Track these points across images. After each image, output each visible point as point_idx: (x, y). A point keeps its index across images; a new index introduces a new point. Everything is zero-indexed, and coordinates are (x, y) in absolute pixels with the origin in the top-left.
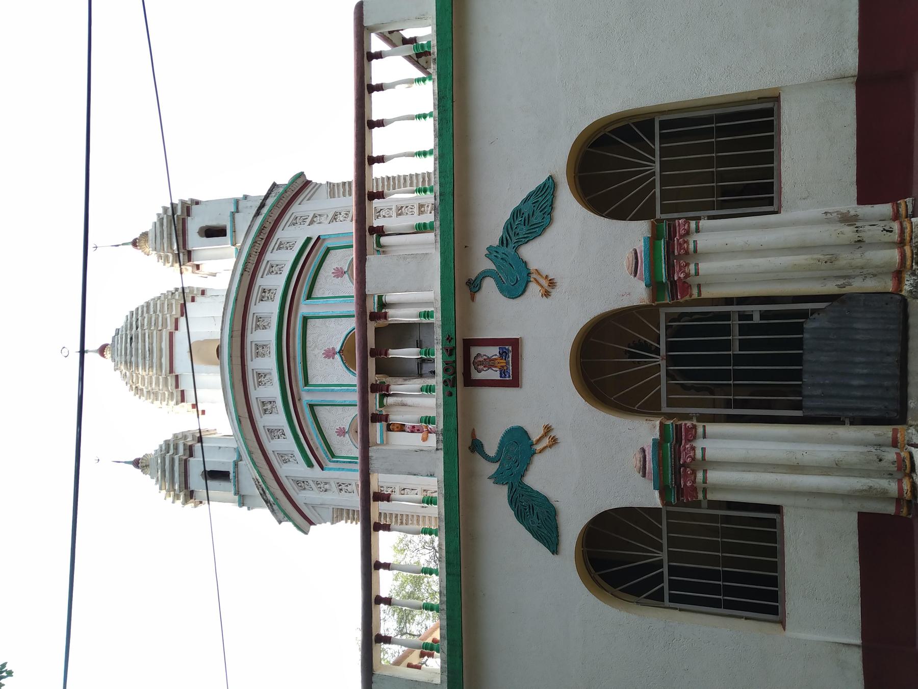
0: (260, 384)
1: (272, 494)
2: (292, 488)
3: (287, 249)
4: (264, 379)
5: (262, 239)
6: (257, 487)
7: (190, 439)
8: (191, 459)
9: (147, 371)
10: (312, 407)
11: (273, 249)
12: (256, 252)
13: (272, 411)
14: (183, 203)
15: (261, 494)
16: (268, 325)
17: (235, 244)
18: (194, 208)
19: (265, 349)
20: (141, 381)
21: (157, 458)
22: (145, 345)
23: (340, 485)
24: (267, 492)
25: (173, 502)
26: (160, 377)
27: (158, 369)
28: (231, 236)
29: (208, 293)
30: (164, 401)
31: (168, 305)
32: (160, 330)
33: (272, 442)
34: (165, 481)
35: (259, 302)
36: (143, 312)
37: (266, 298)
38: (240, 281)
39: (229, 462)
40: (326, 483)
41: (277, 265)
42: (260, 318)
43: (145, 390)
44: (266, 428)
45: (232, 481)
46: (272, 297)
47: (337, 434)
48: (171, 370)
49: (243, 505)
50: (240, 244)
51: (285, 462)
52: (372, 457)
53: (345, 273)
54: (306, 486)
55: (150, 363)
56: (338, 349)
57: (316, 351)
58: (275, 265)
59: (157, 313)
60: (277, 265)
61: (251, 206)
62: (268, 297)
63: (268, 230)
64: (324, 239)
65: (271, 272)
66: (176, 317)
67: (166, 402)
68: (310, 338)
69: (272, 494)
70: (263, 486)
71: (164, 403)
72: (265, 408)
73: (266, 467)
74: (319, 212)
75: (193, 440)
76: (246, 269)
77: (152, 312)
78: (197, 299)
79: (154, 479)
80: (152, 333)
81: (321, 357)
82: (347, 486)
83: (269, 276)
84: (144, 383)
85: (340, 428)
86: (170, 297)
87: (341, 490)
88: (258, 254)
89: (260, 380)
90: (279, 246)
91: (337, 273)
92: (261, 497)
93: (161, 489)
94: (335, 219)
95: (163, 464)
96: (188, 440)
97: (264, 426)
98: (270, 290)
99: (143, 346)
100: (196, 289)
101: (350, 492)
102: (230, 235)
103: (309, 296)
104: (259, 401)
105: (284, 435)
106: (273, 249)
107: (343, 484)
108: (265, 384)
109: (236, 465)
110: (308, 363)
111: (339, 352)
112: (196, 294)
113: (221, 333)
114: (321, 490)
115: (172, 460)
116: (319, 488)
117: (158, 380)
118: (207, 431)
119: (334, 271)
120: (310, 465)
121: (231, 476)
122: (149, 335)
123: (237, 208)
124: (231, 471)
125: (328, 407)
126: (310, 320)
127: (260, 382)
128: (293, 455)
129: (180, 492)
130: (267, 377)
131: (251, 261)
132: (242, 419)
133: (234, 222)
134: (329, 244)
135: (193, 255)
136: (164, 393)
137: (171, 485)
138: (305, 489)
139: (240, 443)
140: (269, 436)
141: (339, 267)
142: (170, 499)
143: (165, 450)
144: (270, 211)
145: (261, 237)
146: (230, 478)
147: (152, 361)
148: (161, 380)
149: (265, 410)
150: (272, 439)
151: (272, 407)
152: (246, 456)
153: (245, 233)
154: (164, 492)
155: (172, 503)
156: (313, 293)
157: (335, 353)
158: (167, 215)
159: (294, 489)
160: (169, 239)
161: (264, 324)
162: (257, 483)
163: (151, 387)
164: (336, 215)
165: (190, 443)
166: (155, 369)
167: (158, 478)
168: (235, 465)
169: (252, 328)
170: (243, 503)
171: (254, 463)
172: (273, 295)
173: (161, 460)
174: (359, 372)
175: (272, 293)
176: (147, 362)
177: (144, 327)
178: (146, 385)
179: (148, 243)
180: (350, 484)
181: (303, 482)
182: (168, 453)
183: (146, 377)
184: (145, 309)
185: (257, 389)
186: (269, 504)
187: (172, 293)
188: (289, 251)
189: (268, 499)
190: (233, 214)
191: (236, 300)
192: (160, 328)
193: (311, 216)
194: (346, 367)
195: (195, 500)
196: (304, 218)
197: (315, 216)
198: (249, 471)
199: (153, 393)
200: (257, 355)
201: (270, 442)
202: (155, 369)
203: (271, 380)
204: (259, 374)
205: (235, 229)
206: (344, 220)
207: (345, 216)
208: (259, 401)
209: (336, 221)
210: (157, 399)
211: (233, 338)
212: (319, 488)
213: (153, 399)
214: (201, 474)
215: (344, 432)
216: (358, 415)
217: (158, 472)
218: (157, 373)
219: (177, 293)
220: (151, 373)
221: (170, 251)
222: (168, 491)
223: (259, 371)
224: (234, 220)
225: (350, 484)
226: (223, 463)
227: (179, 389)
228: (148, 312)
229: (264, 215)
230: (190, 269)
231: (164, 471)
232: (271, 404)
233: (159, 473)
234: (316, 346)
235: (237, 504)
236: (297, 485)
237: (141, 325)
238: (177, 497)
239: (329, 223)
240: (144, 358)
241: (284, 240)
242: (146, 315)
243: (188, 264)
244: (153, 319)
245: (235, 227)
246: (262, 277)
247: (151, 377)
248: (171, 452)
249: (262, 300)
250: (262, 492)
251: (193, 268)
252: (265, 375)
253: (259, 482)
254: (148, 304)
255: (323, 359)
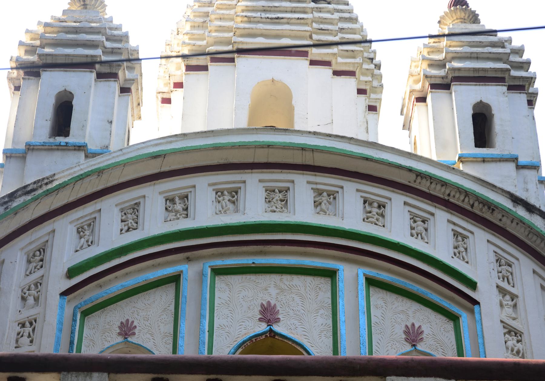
0: (219, 194)
1: (25, 206)
2: (33, 239)
3: (456, 248)
4: (226, 201)
5: (472, 206)
6: (39, 181)
7: (129, 75)
8: (94, 75)
9: (242, 14)
10: (175, 279)
11: (454, 224)
12: (449, 195)
13: (171, 211)
14: (531, 80)
15: (25, 187)
16: (322, 210)
17: (462, 161)
18: (521, 98)
19: (279, 204)
20: (225, 4)
21: (100, 21)
22: (286, 12)
23: (31, 324)
24: (29, 197)
25: (21, 44)
26: (231, 34)
27: (247, 31)
28: (476, 154)
29: (371, 116)
30: (190, 39)
31: (352, 51)
32: (311, 37)
33: (116, 211)
34: (59, 32)
35: (361, 197)
36: (342, 11)
37: (368, 209)
38: (400, 167)
39: (84, 137)
40: (36, 299)
41: (426, 230)
42: (335, 198)
43: (210, 9)
44: (141, 200)
45: (52, 140)
46: (370, 219)
47: (124, 321)
48: (241, 52)
49: (7, 157)
50: (461, 169)
51: (80, 231)
52: (91, 377)
53: (414, 345)
54: (35, 264)
55: (256, 19)
56: (277, 328)
57: (273, 291)
58: (426, 226)
59: (339, 34)
60: (426, 230)
61: (527, 190)
62: (370, 212)
63: (487, 215)
64: (472, 312)
65: (414, 218)
66: (333, 62)
67: (187, 41)
68: (297, 281)
69: (25, 206)
70: (40, 191)
71: (186, 39)
72: (177, 200)
73: (72, 198)
74: (520, 305)
75: (126, 80)
76: (419, 178)
77: (341, 25)
78: (362, 97)
79: (63, 14)
80: (306, 24)
81: (263, 298)
82: (29, 336)
83: (408, 216)
84: (221, 9)
85: (135, 327)
86: (366, 55)
87: (23, 325)
88: (447, 198)
89: (226, 193)
90: (461, 234)
91: (414, 332)
92: (21, 186)
93: (46, 25)
94: (509, 332)
95: (90, 30)
96: (126, 72)
97: (144, 197)
98: (383, 216)
99: (285, 9)
100: (378, 96)
101: (17, 341)
102: (477, 152)
103: (371, 282)
104: (190, 190)
105: (128, 230)
106: (454, 224)
107: (34, 330)
108: (219, 202)
109: (80, 148)
110: (253, 277)
111: (271, 331)
112: (369, 97)
113: (310, 132)
114: (25, 291)
115: (93, 45)
116: (30, 286)
117: (228, 29)
118: (139, 104)
119: (417, 326)
120: (71, 273)
121: (61, 140)
122: (303, 19)
123: (524, 167)
124: (70, 140)
125: (172, 307)
126: (330, 282)
127: (222, 193)
128: (90, 244)
129: (40, 56)
130: (231, 206)
131: (433, 186)
132: (159, 160)
133: (500, 161)
134: (465, 319)
135: (442, 94)
136: (204, 39)
137: (52, 41)
138: (29, 262)
139: (117, 156)
140: (127, 205)
141: (424, 336)
142: (26, 39)
143: (111, 35)
144: (521, 221)
145: (476, 204)
146: (57, 138)
147: (259, 22)
148: (226, 35)
149: (172, 200)
150: (122, 210)
151: (177, 212)
152: (95, 165)
153: (483, 177)
154: (41, 30)
155: (27, 30)
156: (377, 290)
157: (269, 322)
158: (509, 54)
159: (30, 243)
160: (469, 55)
161: (323, 204)
162: (46, 181)
163: (216, 19)
164: (516, 334)
165: (120, 74)
166: (247, 26)
167: (66, 22)
168: (80, 146)
169: (316, 183)
170: (11, 157)
171: (81, 178)
172: (374, 220)
173: (96, 28)
174: (239, 359)
175: (377, 220)
176: (258, 15)
177: (316, 11)
178: (218, 11)
179: (460, 24)
180: (31, 342)
181: (42, 260)
182: (107, 40)
183: (232, 12)
184: (346, 15)
185: (211, 188)
186: (6, 199)
187: (372, 59)
188: (452, 251)
189: (16, 198)
190: (514, 159)
191: (367, 159)
192: (315, 37)
193: (513, 290)
194: (244, 342)
195: (23, 78)
196: (510, 277)
197: (513, 297)
198: (67, 170)
199: (204, 22)
200: (270, 191)
201: (116, 205)
202: (247, 26)
203: (224, 211)
204: (237, 193)
205: (488, 161)
206: (507, 348)
207: (516, 349)
208: (190, 190)
209: (505, 334)
210: (193, 27)
211: (300, 152)
212: (30, 286)
213: (194, 22)
214: (68, 89)
215: (126, 334)
216: (152, 355)
217: (75, 22)
218: (238, 28)
219: (372, 66)
220: (239, 19)
221: (450, 55)
222: (42, 37)
223: (241, 193)
224: (503, 161)
225: (31, 342)
226: (84, 127)
227: (209, 64)
228: (341, 19)
229: (514, 209)
230: (418, 87)
231: (76, 31)
232: (184, 210)
233: (75, 24)
234: (282, 290)
235: (10, 147)
236: (38, 248)
237: (320, 8)
238: (31, 50)
239: (502, 322)
240: (264, 10)
241: (470, 241)
242: (336, 16)
243: (427, 84)
244: (330, 27)
245: (492, 161)
246: (405, 203)
247: (232, 20)
248: (108, 44)
249: (365, 202)
250: (29, 188)
251: (419, 91)
252: (234, 203)
253: (46, 184)
254: (354, 20)
255: (259, 302)
